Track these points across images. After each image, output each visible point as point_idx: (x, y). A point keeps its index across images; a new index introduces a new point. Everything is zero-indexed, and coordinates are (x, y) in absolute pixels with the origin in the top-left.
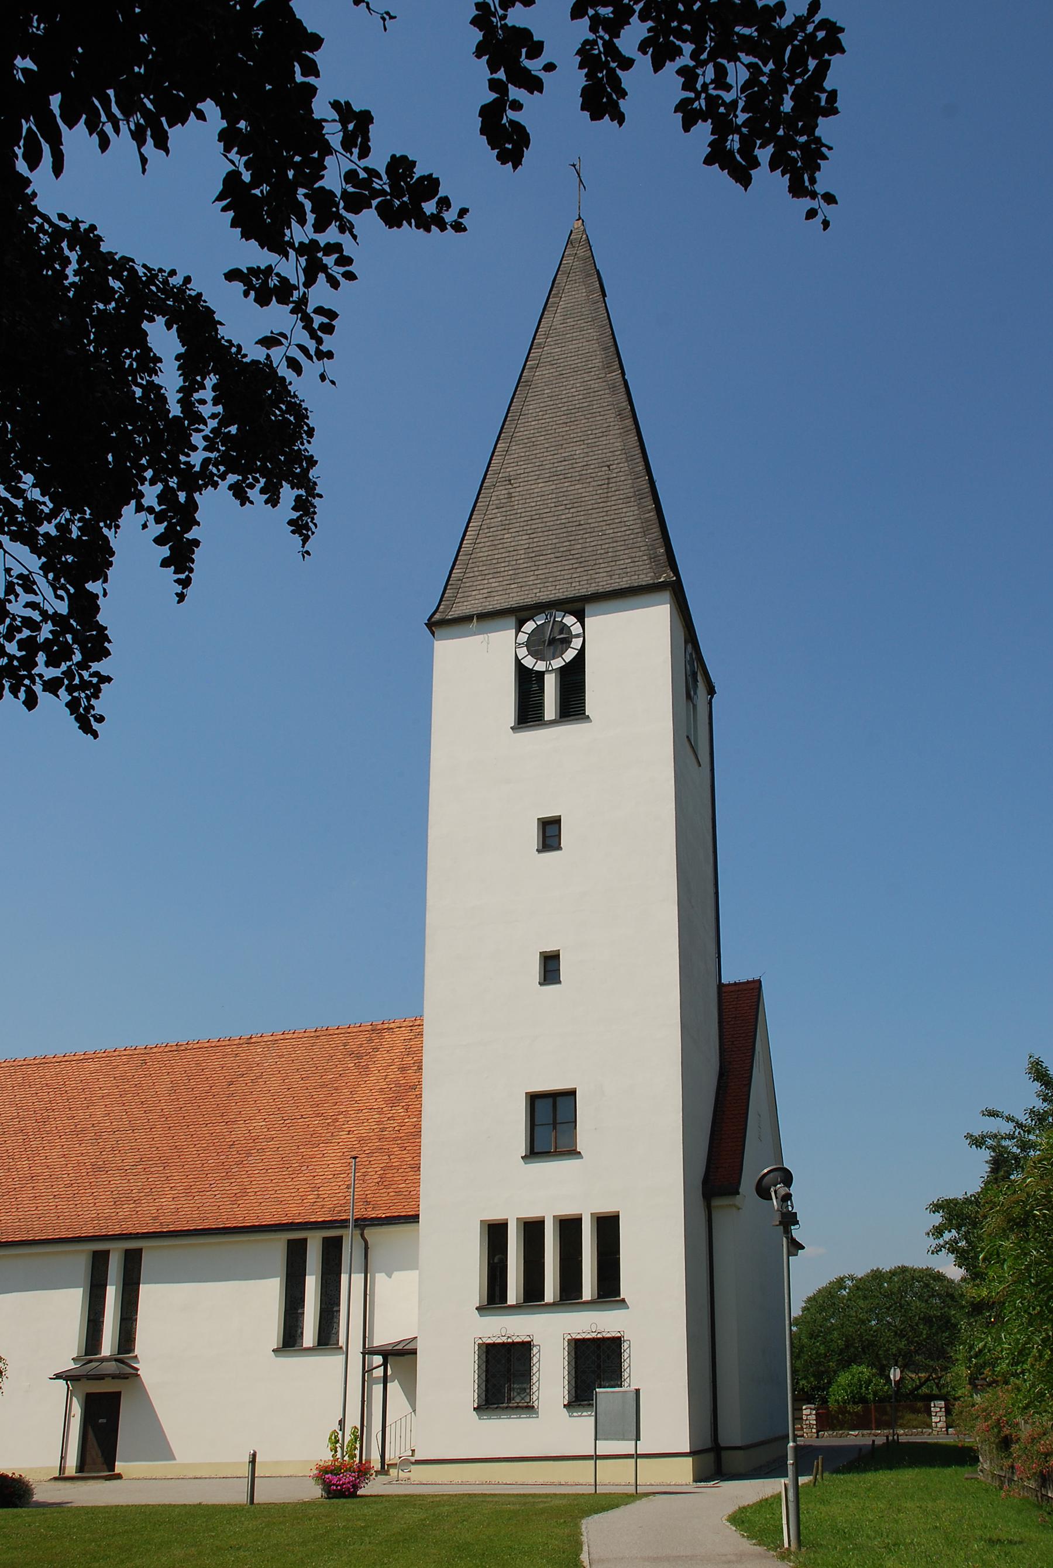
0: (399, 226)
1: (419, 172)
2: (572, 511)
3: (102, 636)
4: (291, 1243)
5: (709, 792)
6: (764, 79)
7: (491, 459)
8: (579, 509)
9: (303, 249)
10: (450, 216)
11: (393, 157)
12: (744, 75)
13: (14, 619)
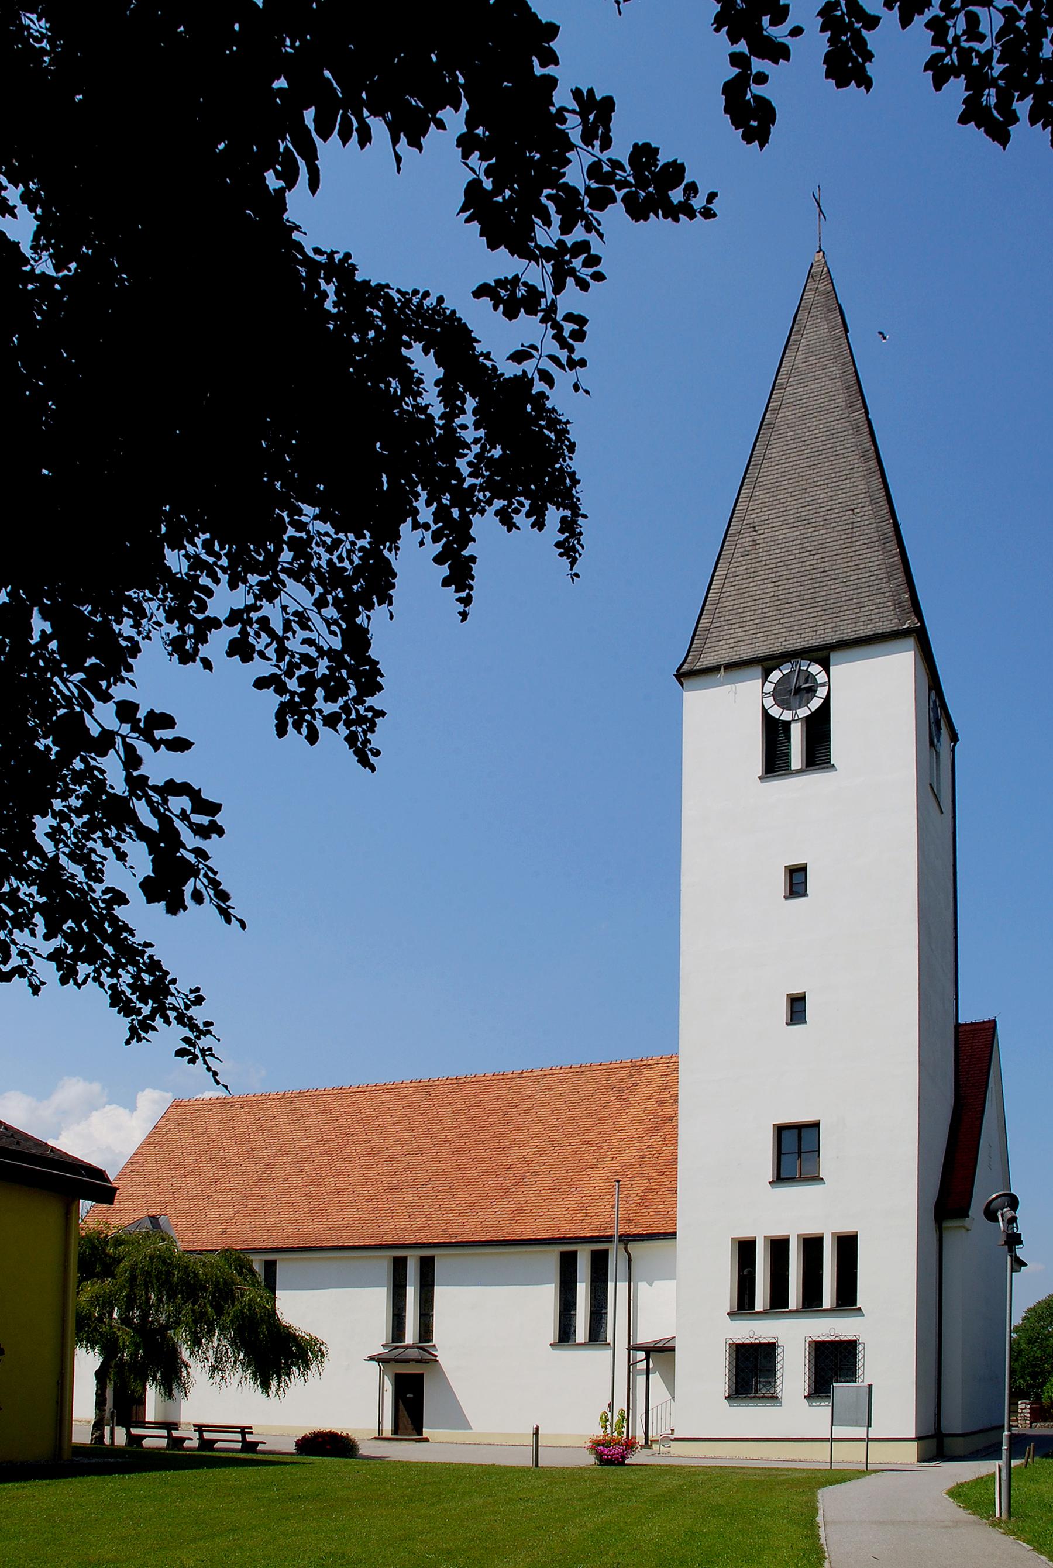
0: (646, 219)
1: (663, 159)
2: (816, 557)
3: (376, 671)
4: (563, 1255)
5: (950, 803)
6: (1021, 24)
7: (735, 506)
8: (824, 555)
9: (547, 254)
10: (698, 202)
11: (636, 145)
12: (999, 21)
13: (292, 656)
